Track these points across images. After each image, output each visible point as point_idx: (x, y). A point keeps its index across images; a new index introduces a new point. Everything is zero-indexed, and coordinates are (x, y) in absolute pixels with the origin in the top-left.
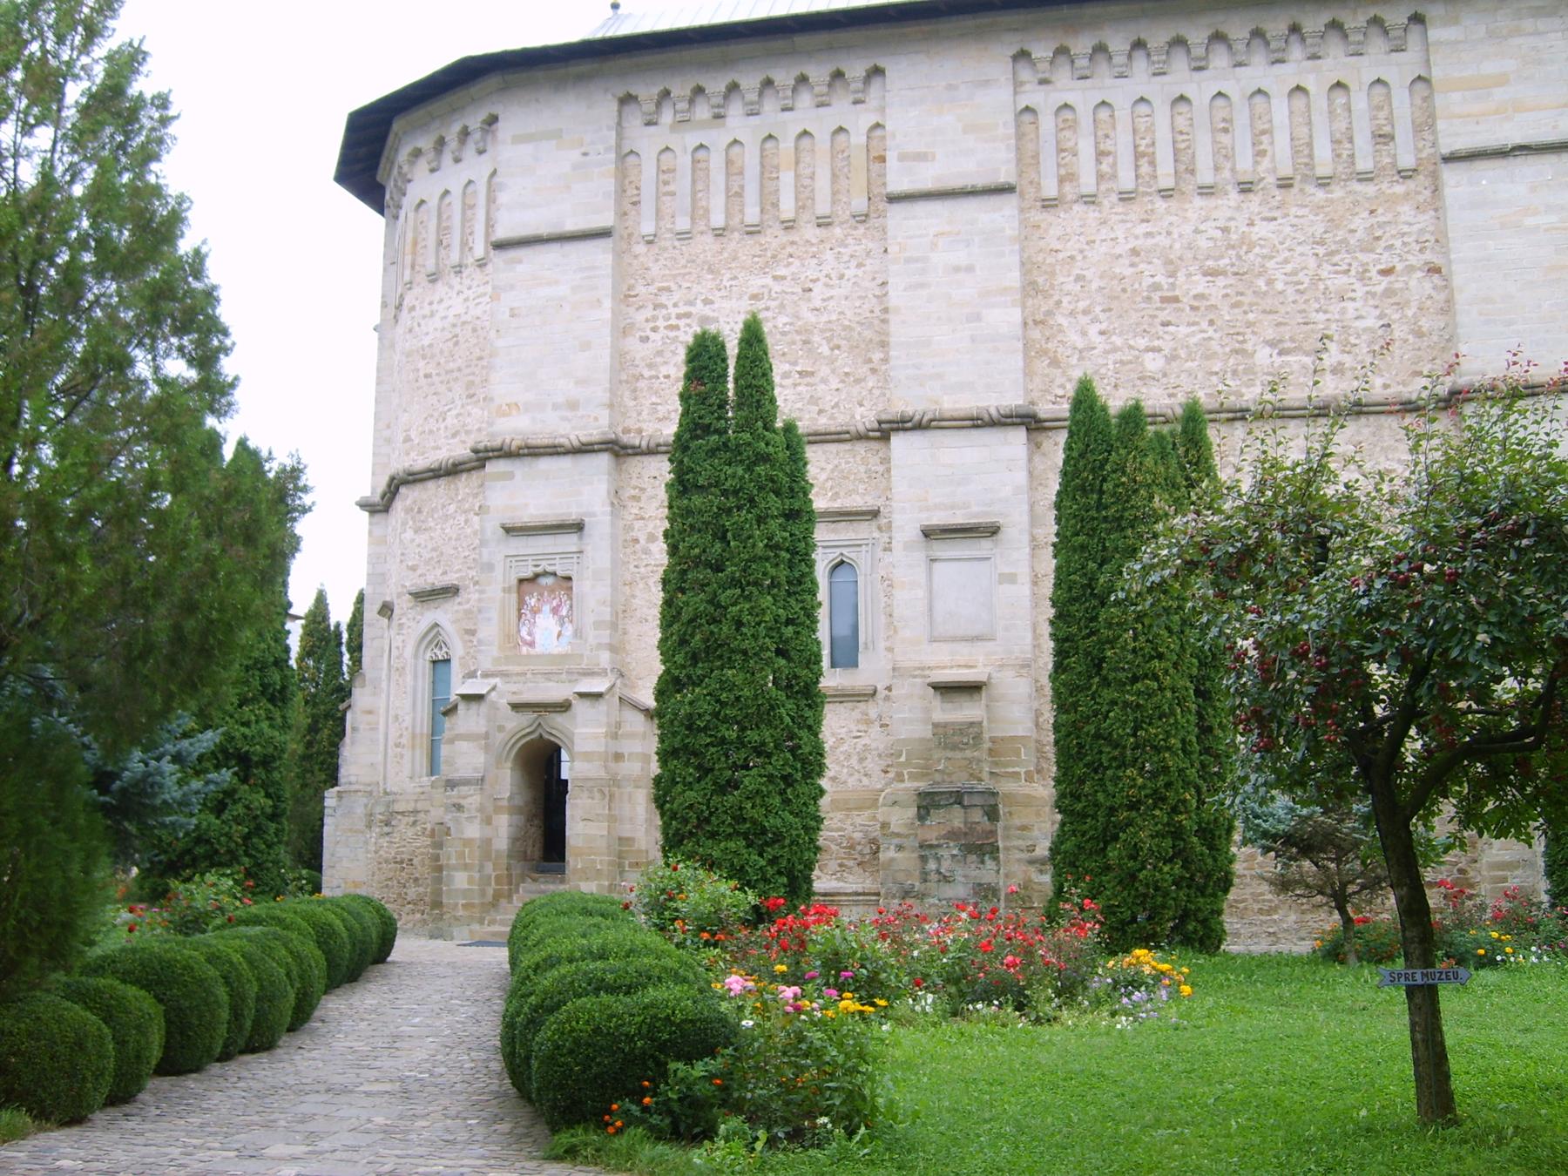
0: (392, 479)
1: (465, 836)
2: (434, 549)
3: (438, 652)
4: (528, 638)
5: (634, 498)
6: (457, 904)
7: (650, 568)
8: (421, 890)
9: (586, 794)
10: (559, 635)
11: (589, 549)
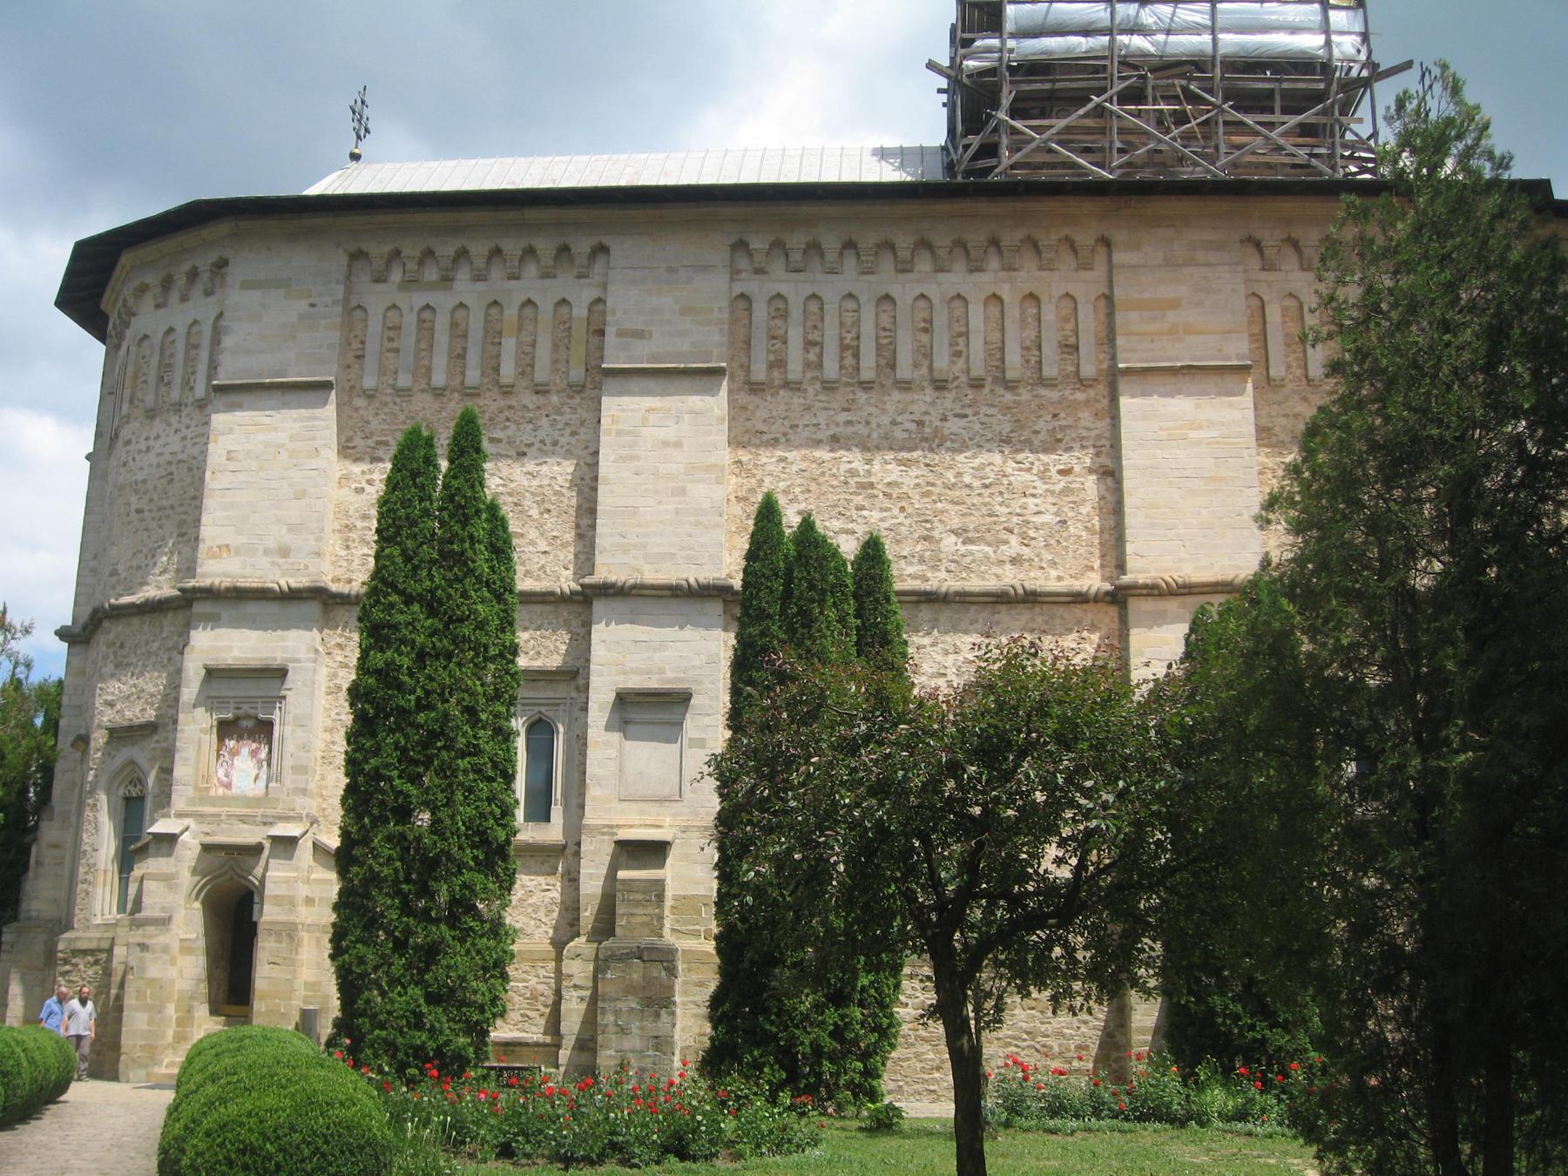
4: (225, 779)
6: (135, 1046)
10: (257, 778)
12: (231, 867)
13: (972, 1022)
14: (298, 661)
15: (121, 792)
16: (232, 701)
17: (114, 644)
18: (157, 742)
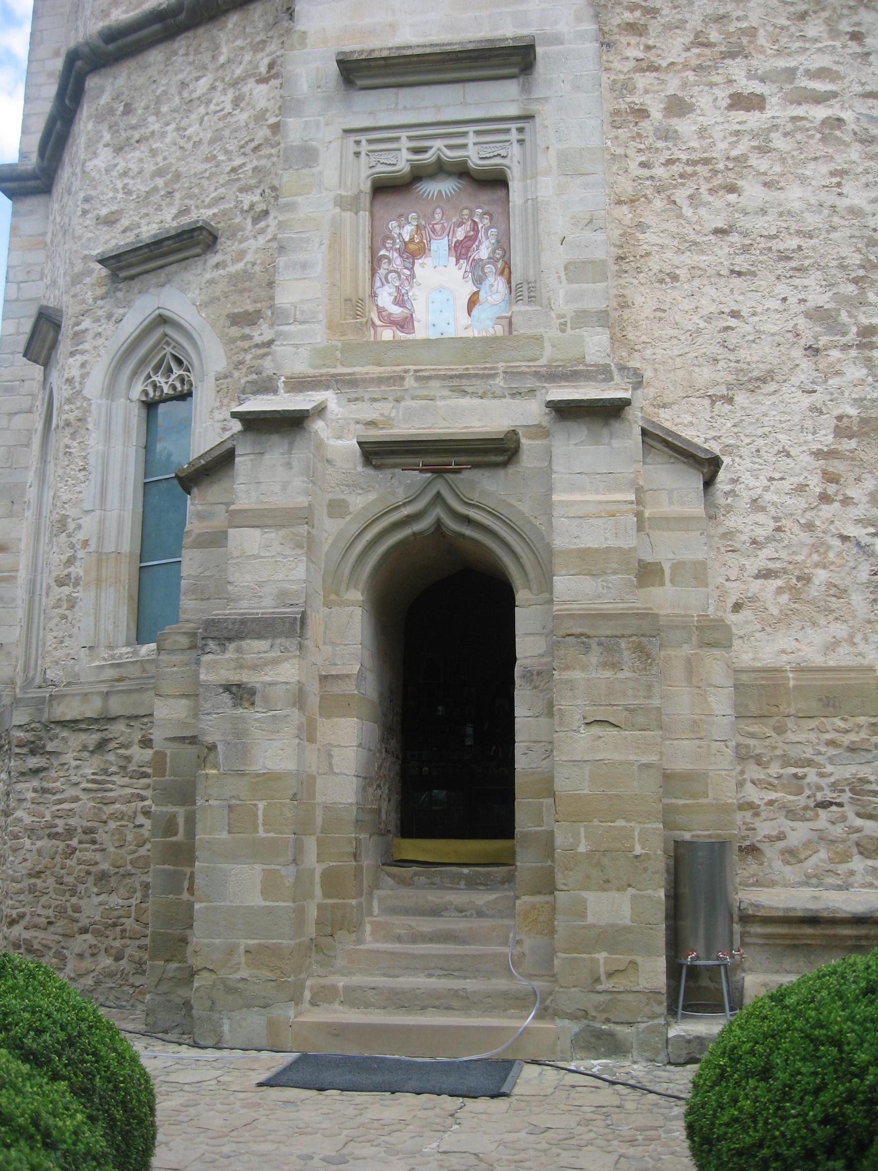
0: (72, 57)
1: (257, 767)
2: (159, 173)
3: (159, 379)
4: (396, 310)
5: (633, 28)
6: (231, 951)
7: (676, 169)
8: (115, 900)
10: (473, 302)
11: (547, 115)
13: (331, 864)
14: (557, 39)
16: (404, 134)
17: (111, 111)
18: (217, 266)
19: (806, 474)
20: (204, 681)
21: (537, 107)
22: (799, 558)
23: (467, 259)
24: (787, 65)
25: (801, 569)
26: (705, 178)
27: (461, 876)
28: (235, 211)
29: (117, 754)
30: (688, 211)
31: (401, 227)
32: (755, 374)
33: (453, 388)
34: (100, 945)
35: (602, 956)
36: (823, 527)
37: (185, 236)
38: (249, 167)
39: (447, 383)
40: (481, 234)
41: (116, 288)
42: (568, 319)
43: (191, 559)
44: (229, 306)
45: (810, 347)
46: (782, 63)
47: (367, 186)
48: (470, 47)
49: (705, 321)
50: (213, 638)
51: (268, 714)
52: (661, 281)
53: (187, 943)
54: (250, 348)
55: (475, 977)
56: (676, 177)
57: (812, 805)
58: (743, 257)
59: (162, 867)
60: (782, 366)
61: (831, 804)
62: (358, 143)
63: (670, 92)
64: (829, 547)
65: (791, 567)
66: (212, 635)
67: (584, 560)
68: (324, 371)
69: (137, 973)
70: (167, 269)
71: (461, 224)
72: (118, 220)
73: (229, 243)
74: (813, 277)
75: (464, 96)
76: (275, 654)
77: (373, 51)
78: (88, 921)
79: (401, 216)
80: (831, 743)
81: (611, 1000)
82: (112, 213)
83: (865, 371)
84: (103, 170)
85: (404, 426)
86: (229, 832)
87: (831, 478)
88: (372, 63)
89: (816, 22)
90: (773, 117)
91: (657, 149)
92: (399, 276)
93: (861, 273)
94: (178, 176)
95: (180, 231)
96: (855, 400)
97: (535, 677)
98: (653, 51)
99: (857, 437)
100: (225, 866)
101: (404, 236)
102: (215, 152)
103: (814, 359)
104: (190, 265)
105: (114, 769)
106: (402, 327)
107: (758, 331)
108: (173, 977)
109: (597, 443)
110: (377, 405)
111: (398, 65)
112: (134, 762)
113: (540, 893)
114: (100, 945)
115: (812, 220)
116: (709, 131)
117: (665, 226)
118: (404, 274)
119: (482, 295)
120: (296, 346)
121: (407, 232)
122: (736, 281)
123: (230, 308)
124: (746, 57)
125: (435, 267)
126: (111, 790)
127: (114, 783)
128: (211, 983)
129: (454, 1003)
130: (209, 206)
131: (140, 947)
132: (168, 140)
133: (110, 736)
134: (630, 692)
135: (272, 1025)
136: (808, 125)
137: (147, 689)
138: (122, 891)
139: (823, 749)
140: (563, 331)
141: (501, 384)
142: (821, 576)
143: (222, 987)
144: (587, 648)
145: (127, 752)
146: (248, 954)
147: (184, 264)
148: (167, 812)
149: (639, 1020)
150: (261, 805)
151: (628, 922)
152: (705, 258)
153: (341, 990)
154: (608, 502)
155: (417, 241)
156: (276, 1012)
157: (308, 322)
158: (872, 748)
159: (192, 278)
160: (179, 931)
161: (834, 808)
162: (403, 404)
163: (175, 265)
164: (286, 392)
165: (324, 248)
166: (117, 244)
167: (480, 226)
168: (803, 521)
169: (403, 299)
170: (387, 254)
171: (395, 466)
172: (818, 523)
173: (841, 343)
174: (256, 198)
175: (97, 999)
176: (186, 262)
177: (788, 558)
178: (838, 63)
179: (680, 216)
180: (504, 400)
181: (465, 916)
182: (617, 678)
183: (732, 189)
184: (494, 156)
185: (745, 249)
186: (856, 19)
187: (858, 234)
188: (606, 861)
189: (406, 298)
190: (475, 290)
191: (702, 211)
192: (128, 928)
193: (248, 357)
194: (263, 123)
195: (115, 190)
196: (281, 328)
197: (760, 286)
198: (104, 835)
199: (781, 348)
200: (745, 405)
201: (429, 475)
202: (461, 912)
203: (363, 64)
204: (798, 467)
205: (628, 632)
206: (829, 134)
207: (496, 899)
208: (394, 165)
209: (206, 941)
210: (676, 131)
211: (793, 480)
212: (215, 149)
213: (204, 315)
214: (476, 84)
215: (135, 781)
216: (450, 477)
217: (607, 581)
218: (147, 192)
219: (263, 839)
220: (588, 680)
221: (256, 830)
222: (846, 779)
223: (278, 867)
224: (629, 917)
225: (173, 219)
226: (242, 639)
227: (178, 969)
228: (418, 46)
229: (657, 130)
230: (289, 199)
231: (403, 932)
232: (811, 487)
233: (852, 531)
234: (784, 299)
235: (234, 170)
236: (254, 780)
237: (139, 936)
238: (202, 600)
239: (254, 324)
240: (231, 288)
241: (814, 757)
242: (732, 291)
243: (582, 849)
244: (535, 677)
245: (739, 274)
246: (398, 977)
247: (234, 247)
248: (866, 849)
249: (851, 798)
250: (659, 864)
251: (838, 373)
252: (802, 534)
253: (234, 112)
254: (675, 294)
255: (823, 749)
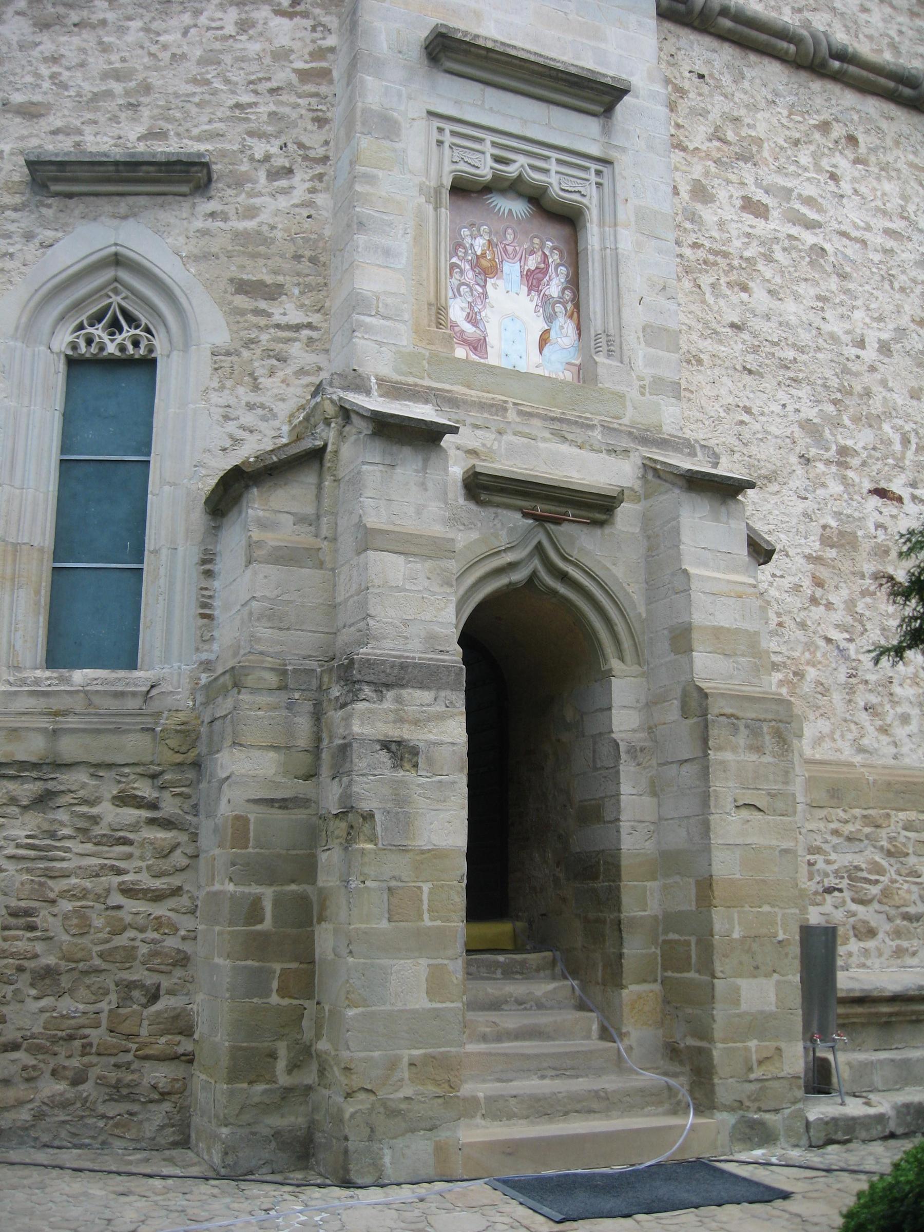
6: (393, 1065)
7: (701, 254)
8: (66, 1005)
9: (741, 740)
10: (544, 340)
12: (539, 548)
15: (63, 339)
16: (489, 138)
18: (213, 215)
19: (800, 575)
20: (358, 734)
21: (615, 154)
22: (796, 654)
23: (539, 292)
24: (785, 184)
25: (796, 665)
26: (724, 271)
27: (497, 964)
28: (241, 156)
29: (73, 812)
30: (710, 299)
31: (473, 237)
32: (763, 472)
33: (554, 431)
34: (42, 1065)
35: (753, 1044)
36: (813, 627)
37: (178, 168)
38: (262, 109)
39: (548, 424)
40: (551, 269)
41: (40, 201)
42: (646, 382)
43: (266, 577)
44: (233, 268)
45: (803, 456)
46: (781, 181)
47: (448, 182)
48: (573, 70)
49: (725, 411)
50: (369, 683)
51: (433, 779)
52: (689, 362)
53: (276, 1058)
54: (267, 327)
55: (587, 1076)
56: (701, 262)
57: (821, 890)
58: (753, 356)
59: (243, 963)
60: (783, 469)
61: (835, 889)
62: (440, 130)
63: (695, 177)
64: (817, 647)
65: (789, 662)
66: (367, 679)
67: (718, 638)
68: (411, 380)
69: (112, 1099)
70: (131, 200)
71: (532, 253)
72: (42, 115)
73: (230, 192)
74: (804, 391)
75: (549, 118)
76: (439, 708)
77: (477, 36)
78: (19, 1034)
79: (473, 225)
80: (835, 832)
81: (761, 1088)
82: (33, 103)
83: (842, 488)
84: (14, 43)
85: (506, 462)
86: (389, 921)
87: (819, 583)
88: (473, 49)
89: (806, 152)
90: (775, 230)
91: (685, 229)
92: (471, 290)
93: (839, 396)
94: (147, 88)
95: (175, 159)
96: (835, 513)
97: (639, 754)
98: (682, 130)
99: (836, 547)
100: (385, 962)
101: (476, 248)
102: (209, 76)
103: (806, 468)
104: (170, 204)
105: (66, 831)
106: (475, 349)
107: (766, 432)
108: (260, 1103)
109: (717, 520)
110: (479, 433)
111: (498, 61)
112: (104, 823)
113: (645, 981)
114: (42, 1065)
115: (805, 337)
116: (727, 226)
117: (693, 307)
118: (476, 290)
119: (553, 334)
120: (380, 344)
121: (479, 244)
122: (747, 379)
123: (233, 271)
124: (755, 165)
125: (508, 292)
126: (63, 859)
127: (67, 850)
128: (369, 1106)
129: (595, 1106)
130: (199, 139)
131: (117, 1066)
132: (130, 38)
133: (62, 788)
134: (771, 777)
135: (440, 1150)
136: (801, 247)
137: (128, 731)
138: (82, 992)
139: (829, 838)
140: (643, 394)
141: (599, 437)
142: (812, 673)
143: (382, 1110)
144: (735, 729)
145: (94, 811)
146: (413, 1067)
147: (160, 199)
148: (250, 894)
149: (784, 1106)
150: (426, 888)
151: (773, 1008)
152: (723, 349)
153: (482, 1101)
154: (736, 583)
155: (489, 258)
156: (443, 1135)
157: (390, 318)
158: (863, 838)
159: (172, 220)
160: (266, 1044)
161: (836, 894)
162: (505, 437)
163: (146, 198)
164: (381, 396)
165: (409, 238)
166: (40, 146)
167: (550, 260)
168: (798, 620)
169: (476, 318)
170: (459, 263)
171: (498, 505)
172: (809, 623)
173: (825, 458)
174: (274, 150)
175: (36, 1139)
176: (163, 198)
177: (786, 653)
178: (821, 196)
179: (704, 302)
180: (601, 455)
181: (525, 1009)
182: (761, 762)
183: (745, 288)
184: (575, 192)
185: (755, 350)
186: (834, 161)
187: (836, 359)
188: (755, 946)
189: (478, 318)
190: (547, 328)
191: (722, 302)
192: (95, 1042)
193: (264, 337)
194: (286, 64)
195: (38, 75)
196: (362, 318)
197: (766, 388)
198: (51, 919)
199: (782, 451)
200: (756, 501)
201: (531, 521)
202: (521, 1004)
203: (464, 47)
204: (794, 567)
205: (770, 717)
206: (816, 260)
207: (555, 989)
208: (477, 167)
209: (363, 1054)
210: (700, 217)
211: (791, 579)
212: (207, 72)
213: (192, 270)
214: (559, 108)
215: (106, 848)
216: (551, 527)
217: (737, 662)
218: (95, 94)
219: (429, 928)
220: (738, 762)
221: (420, 917)
222: (845, 867)
223: (446, 962)
224: (774, 1002)
225: (139, 139)
226: (402, 686)
227: (265, 1092)
228: (523, 49)
229: (685, 210)
230: (368, 169)
231: (488, 1030)
232: (805, 588)
233: (835, 635)
234: (784, 406)
235: (238, 106)
236: (418, 858)
237: (116, 1051)
238: (280, 629)
239: (274, 299)
240: (237, 248)
241: (822, 845)
242: (744, 386)
243: (736, 935)
244: (639, 754)
245: (750, 372)
246: (511, 1081)
247: (239, 199)
248: (860, 932)
249: (849, 884)
250: (795, 950)
251: (823, 485)
252: (798, 632)
253: (238, 37)
254: (700, 377)
255: (829, 838)
